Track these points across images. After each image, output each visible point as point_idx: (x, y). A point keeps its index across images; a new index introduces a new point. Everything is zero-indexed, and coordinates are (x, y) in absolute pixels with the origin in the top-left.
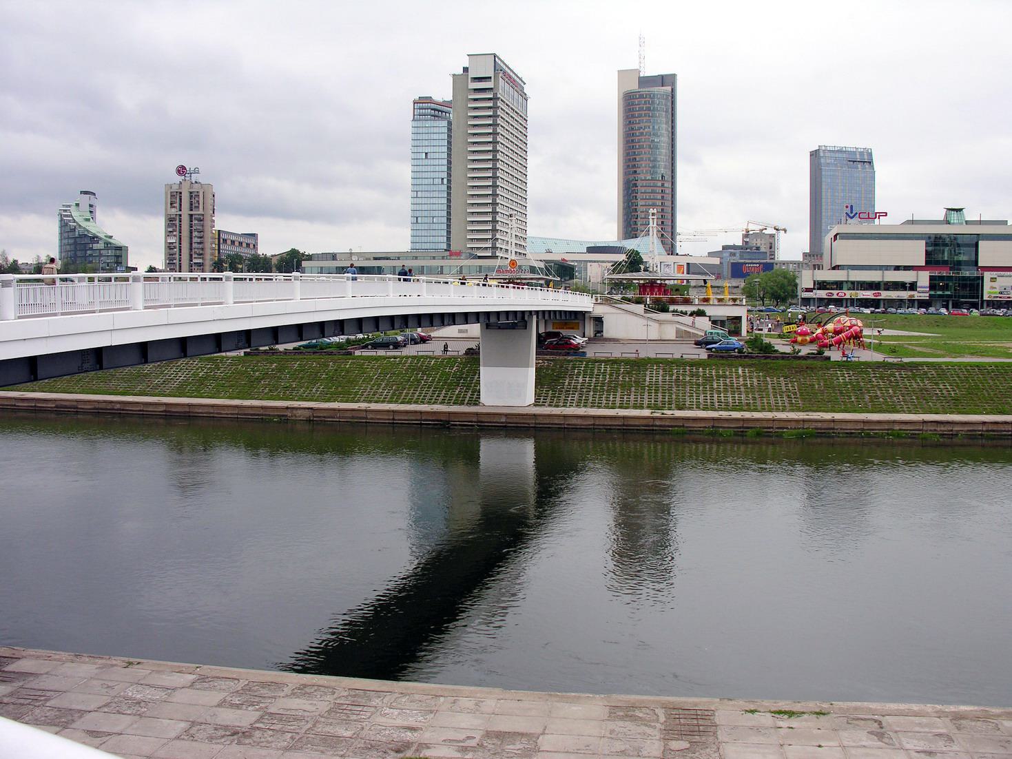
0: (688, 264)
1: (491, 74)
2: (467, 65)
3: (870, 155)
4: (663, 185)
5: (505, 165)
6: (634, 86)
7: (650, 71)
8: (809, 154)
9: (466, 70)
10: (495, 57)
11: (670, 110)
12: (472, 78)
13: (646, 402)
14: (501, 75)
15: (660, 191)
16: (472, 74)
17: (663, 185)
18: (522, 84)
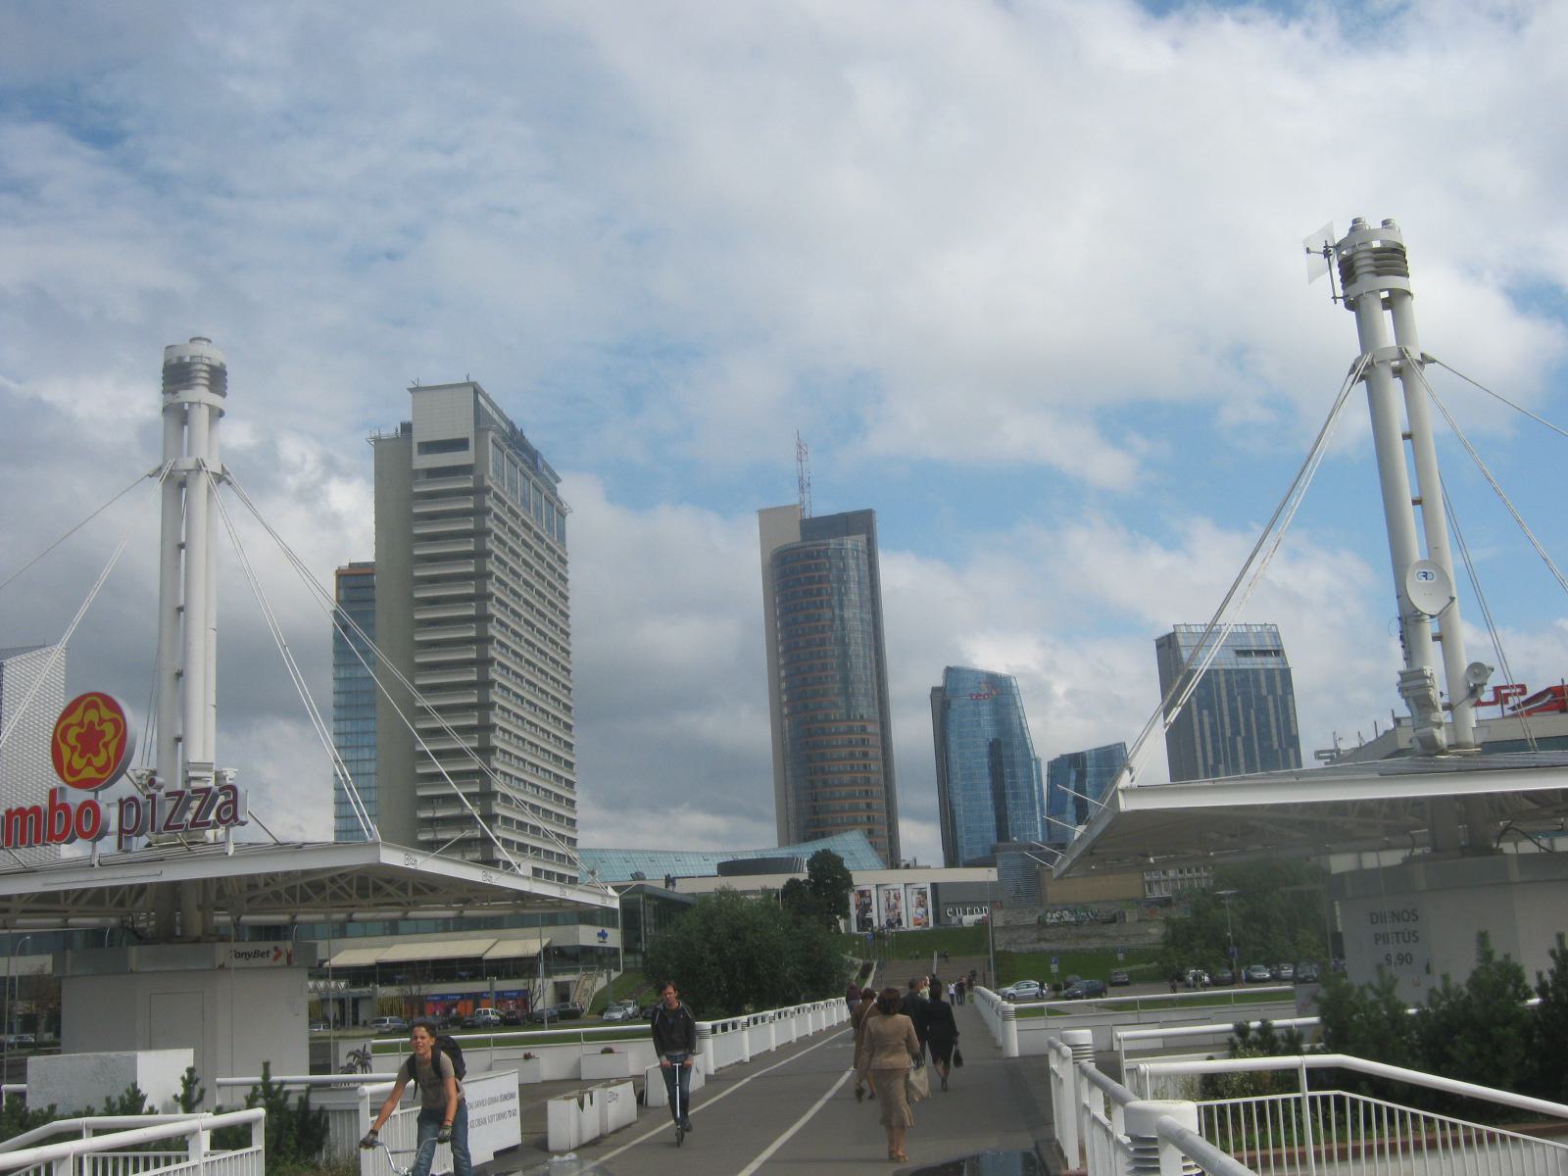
0: (934, 886)
1: (465, 429)
2: (408, 418)
3: (1276, 636)
4: (869, 806)
5: (527, 726)
6: (792, 536)
7: (822, 507)
8: (1122, 741)
9: (406, 428)
10: (476, 392)
11: (867, 580)
12: (420, 445)
13: (1187, 882)
14: (491, 435)
15: (865, 819)
16: (419, 436)
17: (869, 806)
18: (553, 481)
